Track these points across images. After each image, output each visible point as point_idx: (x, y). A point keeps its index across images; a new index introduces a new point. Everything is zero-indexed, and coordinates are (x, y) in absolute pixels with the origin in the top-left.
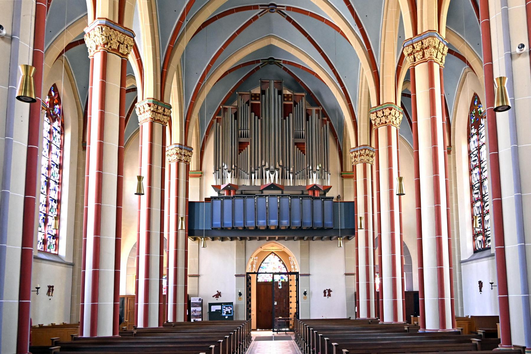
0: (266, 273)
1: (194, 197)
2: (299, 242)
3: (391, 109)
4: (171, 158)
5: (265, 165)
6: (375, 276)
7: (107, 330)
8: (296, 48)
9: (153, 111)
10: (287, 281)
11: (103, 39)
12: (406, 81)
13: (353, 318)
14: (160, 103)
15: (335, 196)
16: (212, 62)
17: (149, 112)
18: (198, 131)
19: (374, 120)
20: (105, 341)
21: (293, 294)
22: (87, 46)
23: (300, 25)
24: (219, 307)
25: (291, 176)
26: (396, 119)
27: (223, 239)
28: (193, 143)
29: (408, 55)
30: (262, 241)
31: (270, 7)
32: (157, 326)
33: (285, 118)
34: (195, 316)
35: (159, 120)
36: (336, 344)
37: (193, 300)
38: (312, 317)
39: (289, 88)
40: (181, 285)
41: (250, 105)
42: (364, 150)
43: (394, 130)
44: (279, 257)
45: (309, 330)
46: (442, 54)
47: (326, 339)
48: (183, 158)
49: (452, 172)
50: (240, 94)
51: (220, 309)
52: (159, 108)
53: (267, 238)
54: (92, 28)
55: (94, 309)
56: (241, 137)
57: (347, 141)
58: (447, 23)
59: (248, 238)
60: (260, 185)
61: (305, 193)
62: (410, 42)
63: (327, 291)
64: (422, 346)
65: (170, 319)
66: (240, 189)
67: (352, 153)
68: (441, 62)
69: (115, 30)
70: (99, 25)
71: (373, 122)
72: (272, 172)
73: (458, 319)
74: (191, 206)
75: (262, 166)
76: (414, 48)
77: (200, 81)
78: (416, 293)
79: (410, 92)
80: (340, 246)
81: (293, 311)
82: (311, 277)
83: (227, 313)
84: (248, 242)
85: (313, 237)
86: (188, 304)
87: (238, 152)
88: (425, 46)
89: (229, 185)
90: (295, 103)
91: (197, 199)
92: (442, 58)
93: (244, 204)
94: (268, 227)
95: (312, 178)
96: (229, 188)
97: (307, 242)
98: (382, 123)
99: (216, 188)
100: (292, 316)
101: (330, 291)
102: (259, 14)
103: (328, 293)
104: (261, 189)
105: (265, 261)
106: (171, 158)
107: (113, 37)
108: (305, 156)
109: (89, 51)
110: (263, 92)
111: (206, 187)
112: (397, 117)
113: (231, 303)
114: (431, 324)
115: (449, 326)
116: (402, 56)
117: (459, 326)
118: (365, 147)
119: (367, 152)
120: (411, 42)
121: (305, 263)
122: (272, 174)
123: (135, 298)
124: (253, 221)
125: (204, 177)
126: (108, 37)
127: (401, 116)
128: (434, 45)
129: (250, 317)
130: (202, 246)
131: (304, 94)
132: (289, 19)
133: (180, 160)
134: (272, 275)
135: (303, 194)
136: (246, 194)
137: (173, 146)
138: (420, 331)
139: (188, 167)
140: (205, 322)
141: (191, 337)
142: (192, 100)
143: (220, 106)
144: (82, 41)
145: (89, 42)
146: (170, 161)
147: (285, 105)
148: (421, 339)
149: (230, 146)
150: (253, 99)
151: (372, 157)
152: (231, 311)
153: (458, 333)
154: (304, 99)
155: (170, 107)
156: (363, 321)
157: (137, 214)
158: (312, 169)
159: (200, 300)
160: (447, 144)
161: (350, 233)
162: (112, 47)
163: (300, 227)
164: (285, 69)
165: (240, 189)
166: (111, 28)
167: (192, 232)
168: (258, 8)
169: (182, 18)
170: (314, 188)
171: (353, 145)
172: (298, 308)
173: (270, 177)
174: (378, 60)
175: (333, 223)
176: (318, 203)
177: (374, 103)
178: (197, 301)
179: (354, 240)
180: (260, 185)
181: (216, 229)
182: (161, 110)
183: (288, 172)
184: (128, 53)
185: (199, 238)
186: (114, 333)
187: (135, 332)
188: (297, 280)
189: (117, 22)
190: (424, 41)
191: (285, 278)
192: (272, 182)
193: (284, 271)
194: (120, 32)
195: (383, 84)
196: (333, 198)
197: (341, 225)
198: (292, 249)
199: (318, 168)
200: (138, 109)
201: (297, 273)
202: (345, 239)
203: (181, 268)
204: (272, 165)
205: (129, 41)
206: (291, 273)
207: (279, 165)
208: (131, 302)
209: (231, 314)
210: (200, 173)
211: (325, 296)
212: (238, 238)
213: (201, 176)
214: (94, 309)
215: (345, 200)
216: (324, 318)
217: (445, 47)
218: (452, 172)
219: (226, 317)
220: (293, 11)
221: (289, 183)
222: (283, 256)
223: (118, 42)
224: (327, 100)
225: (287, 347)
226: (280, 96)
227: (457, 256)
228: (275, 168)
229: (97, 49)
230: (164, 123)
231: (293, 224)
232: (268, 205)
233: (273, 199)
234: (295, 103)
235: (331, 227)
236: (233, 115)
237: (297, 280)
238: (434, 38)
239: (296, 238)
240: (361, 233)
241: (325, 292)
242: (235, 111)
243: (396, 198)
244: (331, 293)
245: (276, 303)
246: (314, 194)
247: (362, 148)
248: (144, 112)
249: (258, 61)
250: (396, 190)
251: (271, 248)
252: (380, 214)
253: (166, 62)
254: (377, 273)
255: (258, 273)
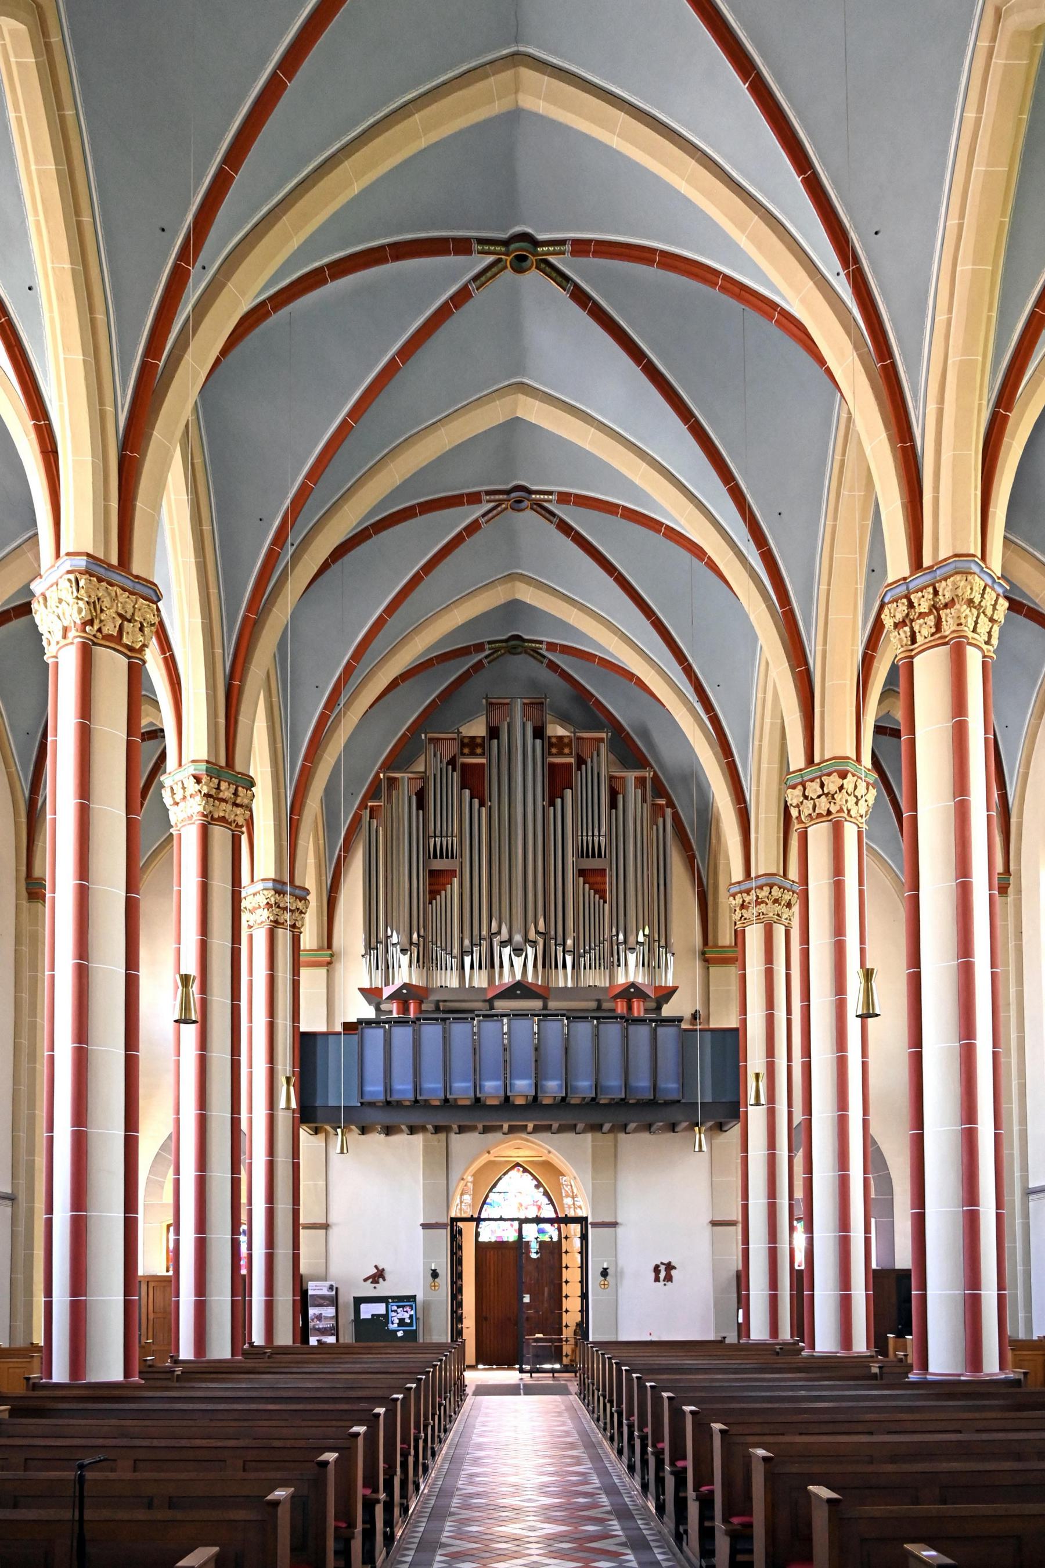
0: (501, 1219)
1: (312, 1022)
2: (589, 1136)
3: (843, 775)
4: (256, 919)
5: (499, 933)
6: (792, 1229)
7: (109, 1365)
8: (583, 608)
9: (207, 796)
10: (555, 1239)
11: (80, 611)
12: (889, 692)
13: (732, 1338)
14: (225, 774)
15: (686, 1012)
16: (358, 655)
17: (198, 798)
18: (321, 842)
19: (798, 806)
20: (105, 1393)
21: (572, 1275)
22: (41, 629)
23: (601, 548)
24: (380, 1309)
25: (569, 959)
26: (857, 804)
27: (389, 1131)
28: (310, 878)
29: (896, 625)
30: (490, 1136)
31: (513, 495)
32: (227, 1355)
33: (552, 804)
34: (319, 1330)
35: (223, 819)
36: (693, 1408)
37: (314, 1289)
38: (623, 1337)
39: (564, 719)
40: (283, 1251)
41: (458, 768)
42: (767, 889)
43: (850, 833)
44: (535, 1178)
45: (619, 1371)
46: (992, 620)
47: (665, 1395)
48: (287, 916)
49: (1011, 945)
50: (431, 740)
51: (384, 1312)
52: (224, 786)
53: (506, 1127)
54: (52, 579)
55: (78, 1314)
56: (435, 857)
57: (722, 862)
58: (1009, 525)
59: (455, 1127)
60: (485, 985)
61: (606, 1005)
62: (902, 590)
63: (662, 1268)
64: (917, 1416)
65: (258, 1338)
66: (434, 997)
67: (734, 896)
68: (987, 643)
69: (111, 584)
70: (69, 572)
71: (794, 812)
72: (518, 951)
73: (1018, 1345)
74: (307, 1045)
75: (492, 936)
76: (911, 605)
77: (325, 707)
78: (905, 1274)
79: (899, 724)
80: (701, 1150)
81: (571, 1317)
82: (620, 1230)
83: (402, 1322)
84: (453, 1137)
85: (626, 1126)
86: (303, 1300)
87: (427, 897)
88: (942, 600)
89: (405, 986)
90: (581, 761)
91: (322, 1028)
92: (989, 633)
93: (444, 1038)
94: (507, 1098)
95: (626, 965)
96: (405, 995)
97: (611, 1136)
98: (820, 815)
99: (371, 994)
100: (567, 1333)
101: (669, 1267)
102: (483, 516)
103: (664, 1272)
104: (490, 996)
105: (500, 1187)
106: (256, 919)
107: (107, 602)
108: (607, 906)
109: (45, 643)
110: (494, 732)
111: (344, 993)
112: (861, 796)
113: (413, 1298)
114: (943, 1359)
115: (991, 1365)
116: (878, 626)
117: (1017, 1365)
118: (771, 880)
119: (776, 892)
120: (904, 587)
121: (605, 1194)
122: (519, 956)
123: (171, 1284)
124: (470, 1084)
125: (340, 968)
126: (94, 605)
127: (873, 792)
128: (967, 595)
129: (460, 1333)
130: (338, 1150)
131: (604, 735)
132: (565, 528)
133: (276, 922)
134: (516, 1224)
135: (599, 1008)
136: (449, 1012)
137: (260, 886)
138: (913, 1377)
139: (296, 941)
140: (347, 1346)
141: (319, 1385)
142: (305, 759)
143: (378, 774)
144: (25, 609)
145: (44, 618)
146: (250, 927)
147: (552, 766)
148: (911, 1397)
149: (406, 882)
150: (466, 751)
151: (789, 905)
152: (411, 1317)
153: (1017, 1383)
154: (603, 748)
155: (251, 783)
156: (759, 1346)
157: (172, 1066)
158: (625, 942)
159: (331, 1288)
160: (999, 867)
161: (727, 1112)
162: (105, 631)
163: (593, 1099)
164: (553, 666)
165: (434, 997)
166: (100, 580)
167: (308, 1114)
168: (480, 501)
169: (280, 538)
170: (631, 992)
171: (737, 873)
172: (584, 1310)
173: (512, 965)
174: (809, 640)
175: (679, 1088)
176: (641, 1034)
177: (797, 760)
178: (325, 1292)
179: (736, 1130)
180: (485, 985)
181: (372, 1104)
182: (227, 793)
183: (560, 949)
184: (145, 645)
185: (328, 1128)
186: (127, 1373)
187: (179, 1370)
188: (584, 1237)
189: (114, 560)
190: (941, 587)
191: (551, 1232)
192: (518, 977)
193: (548, 1212)
194: (124, 590)
195: (823, 705)
196: (680, 1020)
197: (703, 1093)
198: (570, 1154)
199: (641, 939)
200: (168, 790)
201: (582, 1221)
202: (711, 1129)
203: (283, 1206)
204: (519, 933)
205: (144, 611)
206: (568, 1220)
207: (537, 932)
208: (158, 1293)
209: (411, 1325)
210: (328, 955)
211: (657, 1279)
212: (430, 1127)
213: (329, 963)
214: (78, 1314)
215: (712, 1026)
216: (654, 1338)
217: (1001, 601)
218: (1011, 945)
219: (400, 1334)
220: (575, 504)
221: (563, 979)
222: (546, 1174)
223: (120, 615)
224: (667, 752)
225: (560, 1414)
226: (538, 742)
227: (1017, 1174)
228: (526, 940)
229: (65, 637)
230: (237, 825)
231: (575, 1089)
232: (509, 1039)
233: (520, 1024)
234: (581, 761)
235: (675, 1097)
236: (414, 798)
237: (584, 1237)
238: (970, 578)
239: (580, 1126)
240: (756, 1117)
241: (657, 1270)
242: (419, 784)
243: (853, 1026)
244: (673, 1272)
245: (527, 1299)
246: (630, 1008)
247: (762, 881)
248: (184, 798)
249: (479, 647)
250: (854, 1004)
251: (514, 1153)
252: (809, 1062)
253: (240, 660)
254: (799, 1220)
255: (478, 1220)
